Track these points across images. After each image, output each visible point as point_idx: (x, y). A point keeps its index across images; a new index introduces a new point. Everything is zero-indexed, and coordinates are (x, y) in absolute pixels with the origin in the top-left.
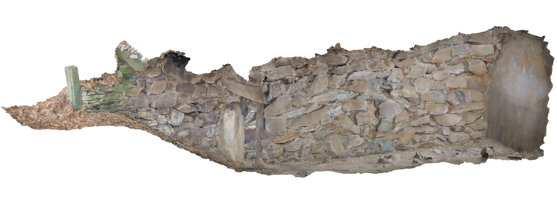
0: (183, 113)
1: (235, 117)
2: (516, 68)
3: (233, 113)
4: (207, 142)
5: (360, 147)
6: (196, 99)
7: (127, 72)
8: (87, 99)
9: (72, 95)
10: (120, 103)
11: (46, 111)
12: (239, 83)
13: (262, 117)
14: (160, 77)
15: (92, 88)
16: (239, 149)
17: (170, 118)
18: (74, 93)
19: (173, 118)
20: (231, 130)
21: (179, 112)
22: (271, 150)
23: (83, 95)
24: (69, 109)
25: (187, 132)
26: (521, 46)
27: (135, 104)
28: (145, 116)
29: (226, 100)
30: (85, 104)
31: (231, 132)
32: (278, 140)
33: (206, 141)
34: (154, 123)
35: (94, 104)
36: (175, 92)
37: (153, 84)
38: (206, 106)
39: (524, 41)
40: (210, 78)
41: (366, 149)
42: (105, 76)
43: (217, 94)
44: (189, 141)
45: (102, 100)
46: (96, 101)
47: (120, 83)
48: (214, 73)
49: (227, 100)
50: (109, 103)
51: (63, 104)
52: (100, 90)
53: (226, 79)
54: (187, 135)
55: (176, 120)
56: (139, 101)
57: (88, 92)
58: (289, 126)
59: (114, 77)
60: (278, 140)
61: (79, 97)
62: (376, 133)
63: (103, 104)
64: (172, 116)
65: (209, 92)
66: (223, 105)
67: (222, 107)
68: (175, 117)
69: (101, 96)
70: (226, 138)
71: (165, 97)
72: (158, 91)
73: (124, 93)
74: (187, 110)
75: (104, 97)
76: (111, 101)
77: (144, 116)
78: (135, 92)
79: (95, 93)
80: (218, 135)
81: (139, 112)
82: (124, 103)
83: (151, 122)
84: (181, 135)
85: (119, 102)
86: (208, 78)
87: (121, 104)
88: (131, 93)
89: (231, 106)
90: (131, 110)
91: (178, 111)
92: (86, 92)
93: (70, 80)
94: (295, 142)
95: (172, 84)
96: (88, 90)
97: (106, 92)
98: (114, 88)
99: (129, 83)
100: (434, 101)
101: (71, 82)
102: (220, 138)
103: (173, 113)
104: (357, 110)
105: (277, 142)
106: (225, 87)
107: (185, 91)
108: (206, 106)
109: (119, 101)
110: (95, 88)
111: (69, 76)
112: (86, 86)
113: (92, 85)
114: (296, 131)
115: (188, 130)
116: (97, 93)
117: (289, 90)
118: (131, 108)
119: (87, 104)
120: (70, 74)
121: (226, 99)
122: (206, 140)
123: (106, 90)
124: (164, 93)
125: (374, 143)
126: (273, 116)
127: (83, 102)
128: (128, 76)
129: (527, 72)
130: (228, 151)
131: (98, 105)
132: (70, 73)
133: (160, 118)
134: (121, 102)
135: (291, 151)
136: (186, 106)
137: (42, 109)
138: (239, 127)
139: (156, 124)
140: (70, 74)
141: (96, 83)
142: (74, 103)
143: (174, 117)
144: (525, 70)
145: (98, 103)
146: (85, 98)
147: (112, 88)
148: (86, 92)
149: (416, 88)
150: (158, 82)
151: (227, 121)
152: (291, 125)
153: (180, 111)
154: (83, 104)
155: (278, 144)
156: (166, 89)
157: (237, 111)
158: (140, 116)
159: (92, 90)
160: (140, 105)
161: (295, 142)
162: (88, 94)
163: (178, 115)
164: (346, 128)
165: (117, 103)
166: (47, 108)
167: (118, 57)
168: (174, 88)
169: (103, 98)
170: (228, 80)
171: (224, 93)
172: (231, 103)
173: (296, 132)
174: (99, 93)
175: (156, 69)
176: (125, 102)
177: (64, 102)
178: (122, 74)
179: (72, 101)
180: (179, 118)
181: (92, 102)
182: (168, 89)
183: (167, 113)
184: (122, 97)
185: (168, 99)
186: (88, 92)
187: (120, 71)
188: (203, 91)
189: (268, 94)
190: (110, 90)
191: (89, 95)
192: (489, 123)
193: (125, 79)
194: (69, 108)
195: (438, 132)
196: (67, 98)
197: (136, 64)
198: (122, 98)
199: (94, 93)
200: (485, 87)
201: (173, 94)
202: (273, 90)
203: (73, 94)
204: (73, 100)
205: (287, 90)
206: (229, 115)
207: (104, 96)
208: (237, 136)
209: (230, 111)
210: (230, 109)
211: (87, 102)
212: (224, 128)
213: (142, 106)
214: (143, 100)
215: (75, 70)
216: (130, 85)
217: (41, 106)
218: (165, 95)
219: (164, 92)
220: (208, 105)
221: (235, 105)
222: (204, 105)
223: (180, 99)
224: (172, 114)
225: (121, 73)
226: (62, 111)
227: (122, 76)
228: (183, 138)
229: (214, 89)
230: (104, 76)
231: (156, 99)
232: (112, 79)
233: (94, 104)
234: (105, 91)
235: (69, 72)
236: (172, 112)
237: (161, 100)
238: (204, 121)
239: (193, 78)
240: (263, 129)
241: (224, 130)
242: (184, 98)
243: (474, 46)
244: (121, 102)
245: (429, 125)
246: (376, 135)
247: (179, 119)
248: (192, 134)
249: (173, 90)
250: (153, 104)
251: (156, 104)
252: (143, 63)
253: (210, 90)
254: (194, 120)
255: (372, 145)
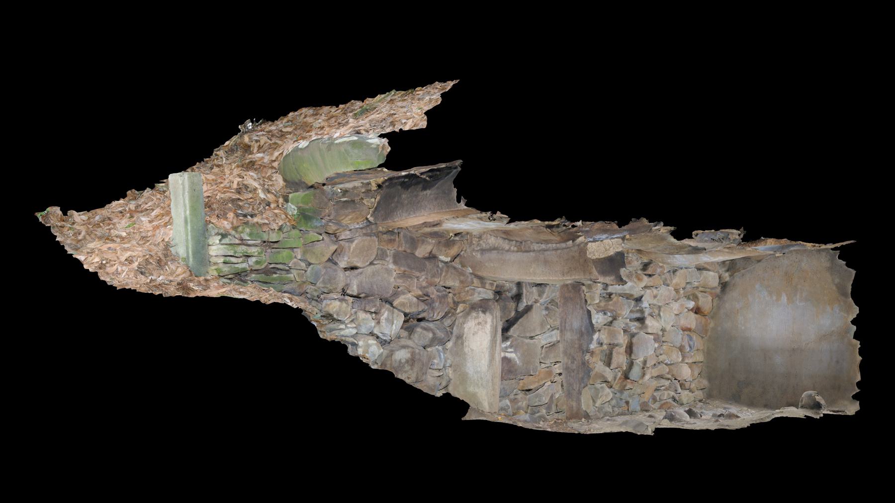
0: (402, 312)
1: (491, 326)
2: (767, 298)
3: (488, 318)
4: (434, 377)
5: (607, 404)
6: (425, 288)
7: (307, 204)
8: (221, 253)
9: (187, 240)
10: (291, 273)
11: (120, 269)
12: (513, 251)
13: (582, 308)
14: (368, 228)
15: (233, 229)
16: (493, 389)
17: (379, 323)
18: (191, 235)
19: (384, 321)
20: (483, 353)
21: (395, 310)
22: (515, 401)
23: (211, 243)
24: (180, 270)
25: (409, 352)
26: (776, 267)
27: (318, 283)
28: (336, 311)
29: (471, 296)
30: (215, 264)
31: (483, 355)
32: (524, 383)
33: (432, 375)
34: (351, 329)
35: (237, 266)
36: (392, 266)
37: (356, 242)
38: (437, 304)
39: (784, 259)
40: (447, 249)
41: (613, 407)
42: (260, 210)
43: (458, 282)
44: (411, 372)
45: (254, 259)
46: (241, 259)
47: (294, 228)
48: (453, 240)
49: (474, 294)
50: (268, 272)
51: (163, 258)
52: (250, 235)
53: (478, 251)
54: (409, 358)
55: (390, 326)
56: (327, 277)
57: (224, 236)
58: (542, 358)
59: (280, 213)
60: (524, 383)
61: (203, 247)
62: (624, 383)
63: (255, 272)
64: (382, 318)
65: (445, 276)
66: (465, 305)
67: (462, 309)
68: (387, 320)
69: (253, 250)
70: (470, 368)
71: (374, 274)
72: (362, 259)
73: (299, 252)
74: (410, 306)
75: (259, 253)
76: (272, 266)
77: (335, 310)
78: (321, 254)
79: (240, 242)
80: (450, 366)
81: (325, 302)
82: (298, 274)
83: (346, 326)
84: (399, 358)
85: (288, 271)
86: (444, 249)
87: (292, 275)
88: (314, 253)
89: (481, 307)
90: (309, 296)
91: (394, 307)
92: (220, 237)
93: (182, 201)
94: (546, 388)
95: (385, 251)
96: (224, 232)
97: (265, 242)
98: (281, 233)
99: (312, 228)
100: (672, 343)
101: (185, 205)
102: (455, 371)
103: (384, 312)
104: (612, 342)
105: (523, 387)
106: (470, 270)
107: (409, 266)
108: (437, 304)
109: (288, 268)
110: (240, 229)
111: (181, 192)
112: (219, 224)
113: (232, 223)
114: (547, 369)
115: (410, 350)
116: (243, 242)
117: (545, 296)
118: (308, 291)
119: (221, 265)
120: (184, 188)
121: (470, 293)
122: (433, 373)
123: (265, 238)
124: (373, 267)
125: (622, 397)
126: (526, 337)
127: (211, 260)
128: (310, 214)
129: (790, 300)
130: (474, 395)
131: (244, 271)
132: (183, 184)
133: (363, 319)
134: (292, 271)
135: (536, 404)
136: (409, 299)
137: (108, 265)
138: (496, 346)
139: (354, 331)
140: (184, 188)
141: (241, 220)
142: (191, 260)
143: (386, 319)
144: (786, 298)
145: (244, 265)
146: (216, 249)
147: (277, 233)
148: (220, 237)
149: (662, 320)
150: (365, 238)
151: (473, 334)
152: (545, 357)
153: (397, 309)
154: (210, 266)
155: (523, 391)
156: (375, 259)
157: (495, 315)
158: (326, 309)
159: (233, 232)
160: (328, 286)
161: (545, 388)
162: (223, 242)
163: (393, 317)
164: (598, 371)
165: (284, 272)
166: (122, 264)
167: (283, 178)
168: (390, 259)
169: (256, 254)
170: (482, 254)
171: (469, 280)
172: (481, 300)
173: (548, 371)
174: (250, 242)
175: (365, 208)
176: (300, 273)
177: (166, 256)
178: (296, 208)
179: (185, 256)
180: (395, 322)
181: (233, 260)
182: (378, 259)
183: (376, 308)
184: (295, 260)
185: (380, 278)
186: (224, 236)
187: (292, 204)
188: (436, 273)
189: (521, 298)
190: (274, 237)
191: (226, 244)
192: (710, 379)
193: (303, 220)
194: (178, 267)
195: (668, 389)
196: (171, 249)
197: (356, 151)
198: (295, 263)
199: (237, 242)
200: (706, 331)
201: (388, 270)
202: (528, 292)
203: (189, 238)
204: (188, 252)
205: (540, 295)
206: (479, 324)
207: (260, 250)
208: (493, 365)
209: (481, 315)
210: (481, 312)
211: (222, 260)
212: (466, 350)
213: (332, 288)
214: (334, 274)
215: (195, 178)
216: (313, 235)
217: (107, 259)
218: (375, 269)
219: (371, 264)
220: (440, 303)
221: (490, 303)
222: (433, 303)
223: (400, 282)
224: (383, 315)
225: (293, 207)
226: (162, 272)
227: (295, 212)
228: (401, 365)
229: (453, 271)
230: (258, 209)
231: (359, 277)
232: (276, 216)
233: (237, 266)
234: (262, 238)
235: (180, 182)
236: (383, 310)
237: (367, 280)
238: (434, 334)
239: (420, 245)
240: (588, 332)
241: (465, 354)
242: (407, 280)
243: (705, 272)
244: (292, 271)
245: (663, 378)
246: (625, 386)
247: (395, 326)
248: (416, 357)
249: (388, 262)
250: (352, 287)
251: (358, 286)
252: (375, 146)
253: (447, 272)
254: (410, 335)
255: (620, 402)
